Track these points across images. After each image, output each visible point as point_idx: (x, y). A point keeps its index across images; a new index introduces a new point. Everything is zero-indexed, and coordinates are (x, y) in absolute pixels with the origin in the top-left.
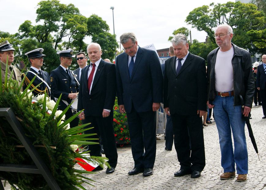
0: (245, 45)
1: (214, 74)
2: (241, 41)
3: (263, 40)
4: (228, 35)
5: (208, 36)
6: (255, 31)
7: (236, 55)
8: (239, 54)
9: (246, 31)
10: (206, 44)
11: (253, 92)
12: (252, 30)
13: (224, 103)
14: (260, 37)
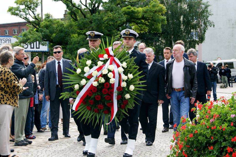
0: (119, 26)
1: (171, 76)
2: (112, 20)
3: (143, 21)
4: (181, 51)
5: (68, 11)
6: (132, 8)
7: (186, 65)
8: (188, 65)
9: (122, 7)
10: (63, 22)
11: (197, 89)
12: (130, 6)
13: (178, 96)
14: (140, 17)
